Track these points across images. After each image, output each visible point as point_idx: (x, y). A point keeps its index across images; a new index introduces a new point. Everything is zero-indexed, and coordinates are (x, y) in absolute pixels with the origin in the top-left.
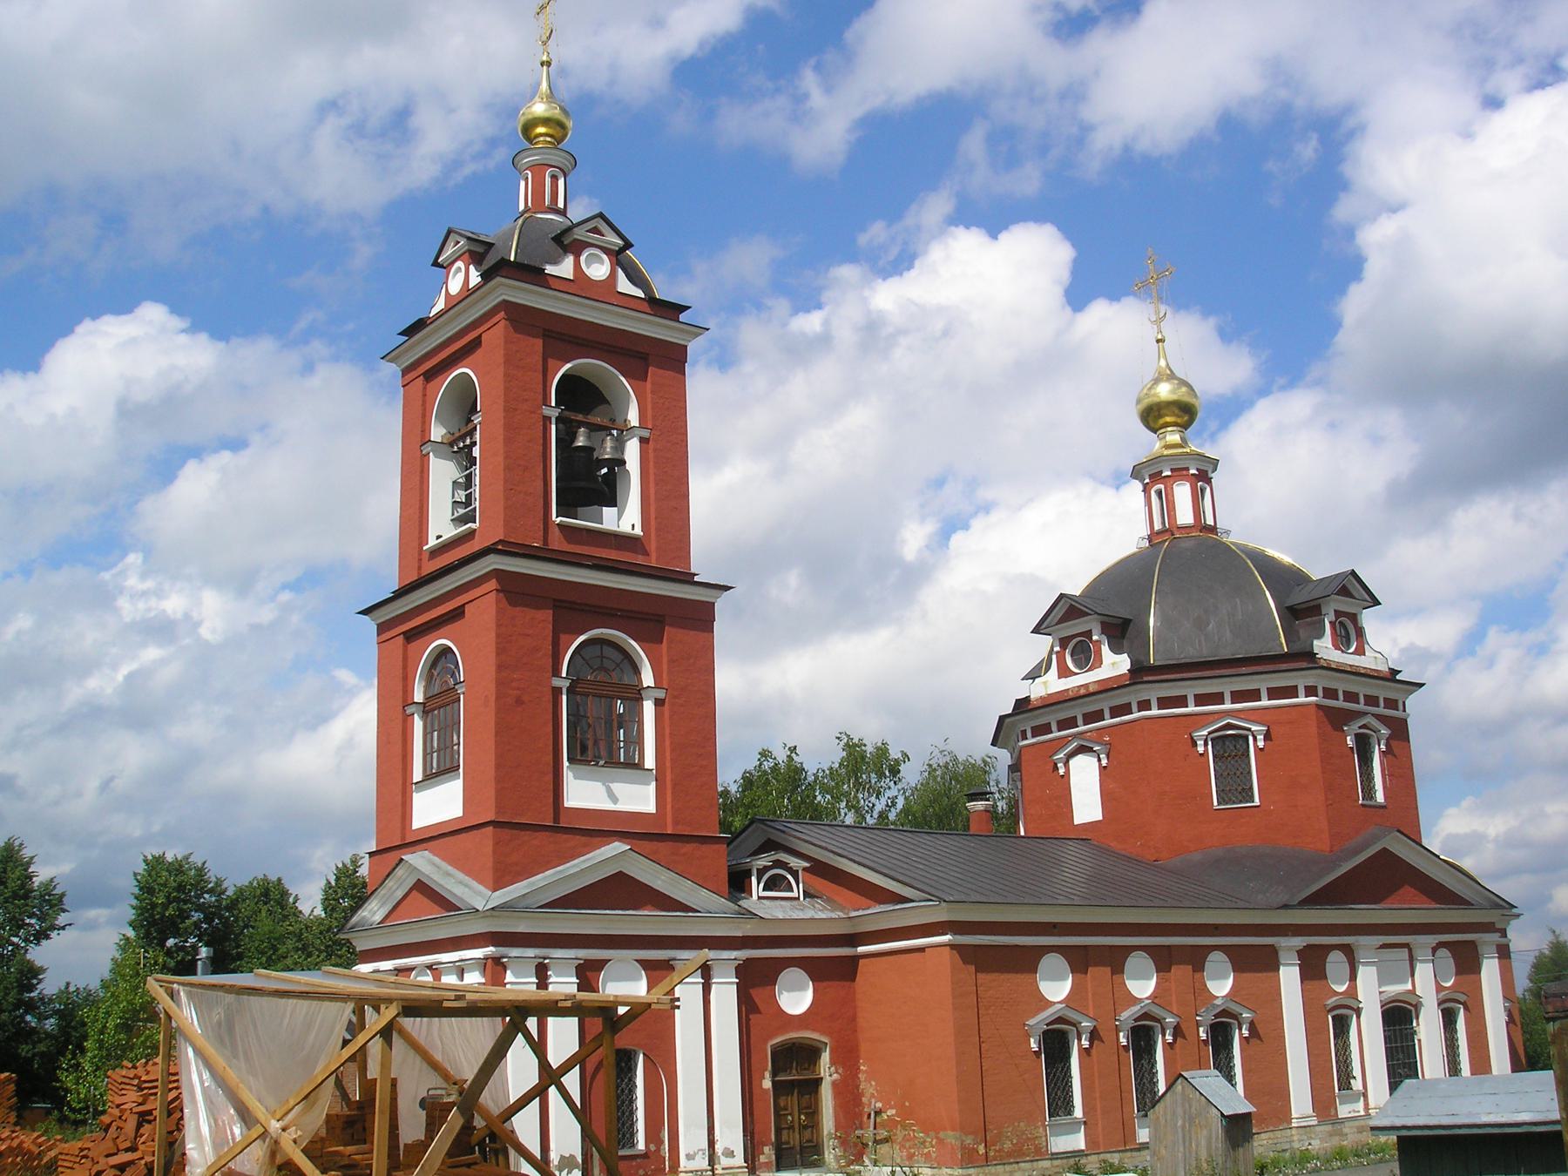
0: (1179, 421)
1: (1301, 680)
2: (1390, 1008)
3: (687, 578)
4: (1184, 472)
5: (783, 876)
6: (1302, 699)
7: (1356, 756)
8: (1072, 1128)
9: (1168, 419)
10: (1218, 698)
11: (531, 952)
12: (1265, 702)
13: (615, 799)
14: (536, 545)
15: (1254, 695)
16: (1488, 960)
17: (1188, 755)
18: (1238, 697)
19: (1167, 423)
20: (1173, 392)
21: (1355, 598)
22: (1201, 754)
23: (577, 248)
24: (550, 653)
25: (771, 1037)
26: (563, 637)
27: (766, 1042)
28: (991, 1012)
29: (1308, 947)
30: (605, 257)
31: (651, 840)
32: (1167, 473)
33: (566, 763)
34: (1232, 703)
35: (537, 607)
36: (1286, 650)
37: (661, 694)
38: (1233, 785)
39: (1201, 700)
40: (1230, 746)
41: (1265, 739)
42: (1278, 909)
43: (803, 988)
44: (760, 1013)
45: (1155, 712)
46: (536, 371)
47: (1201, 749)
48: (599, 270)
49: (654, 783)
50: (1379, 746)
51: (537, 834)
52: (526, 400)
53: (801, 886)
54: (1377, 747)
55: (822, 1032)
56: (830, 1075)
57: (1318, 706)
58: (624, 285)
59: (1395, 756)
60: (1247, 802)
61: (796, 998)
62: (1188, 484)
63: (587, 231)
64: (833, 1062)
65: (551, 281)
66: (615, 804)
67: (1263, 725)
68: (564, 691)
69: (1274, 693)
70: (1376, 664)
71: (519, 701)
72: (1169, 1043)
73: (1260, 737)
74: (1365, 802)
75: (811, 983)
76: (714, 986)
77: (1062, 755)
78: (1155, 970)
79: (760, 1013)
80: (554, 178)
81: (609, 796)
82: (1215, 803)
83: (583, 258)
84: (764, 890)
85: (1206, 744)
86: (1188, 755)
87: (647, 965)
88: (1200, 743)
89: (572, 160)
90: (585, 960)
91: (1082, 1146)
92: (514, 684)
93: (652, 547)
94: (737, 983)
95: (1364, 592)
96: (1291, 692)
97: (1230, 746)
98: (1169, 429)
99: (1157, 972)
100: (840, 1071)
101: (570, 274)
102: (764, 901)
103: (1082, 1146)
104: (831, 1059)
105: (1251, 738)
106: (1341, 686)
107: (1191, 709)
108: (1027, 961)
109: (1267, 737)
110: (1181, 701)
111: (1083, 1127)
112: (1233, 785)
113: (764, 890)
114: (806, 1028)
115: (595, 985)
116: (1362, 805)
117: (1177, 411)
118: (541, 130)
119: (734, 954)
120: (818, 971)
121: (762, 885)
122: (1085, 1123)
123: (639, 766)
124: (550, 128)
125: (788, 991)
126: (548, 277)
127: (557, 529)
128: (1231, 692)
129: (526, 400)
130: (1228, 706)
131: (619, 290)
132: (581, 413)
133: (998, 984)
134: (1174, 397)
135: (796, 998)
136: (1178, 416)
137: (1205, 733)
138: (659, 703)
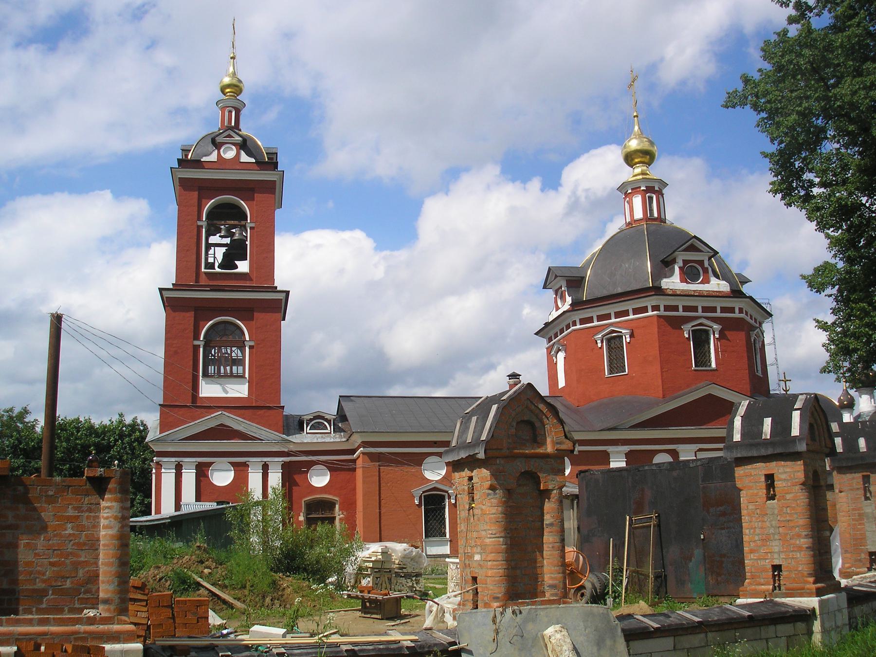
0: (643, 160)
1: (649, 302)
2: (430, 495)
3: (274, 289)
4: (638, 189)
5: (321, 422)
6: (650, 313)
7: (692, 342)
8: (443, 544)
9: (636, 160)
10: (607, 317)
11: (173, 459)
12: (631, 317)
13: (227, 392)
14: (191, 283)
15: (625, 313)
16: (613, 463)
17: (594, 349)
18: (618, 315)
19: (636, 162)
20: (638, 144)
21: (703, 252)
22: (600, 348)
23: (217, 145)
24: (193, 330)
25: (305, 497)
26: (201, 323)
27: (301, 499)
28: (388, 485)
29: (631, 451)
30: (234, 147)
31: (241, 409)
32: (630, 191)
33: (201, 378)
34: (580, 325)
35: (187, 311)
36: (651, 286)
37: (252, 343)
38: (616, 364)
39: (600, 318)
40: (614, 341)
41: (631, 337)
42: (601, 430)
43: (326, 475)
44: (299, 486)
45: (578, 327)
46: (194, 206)
47: (599, 345)
48: (230, 154)
49: (247, 384)
50: (714, 335)
51: (181, 409)
52: (189, 220)
53: (332, 427)
54: (712, 336)
55: (335, 495)
56: (339, 515)
57: (659, 316)
58: (244, 158)
59: (728, 340)
60: (623, 372)
61: (320, 479)
62: (640, 196)
63: (224, 137)
64: (340, 509)
65: (206, 166)
66: (227, 394)
67: (628, 330)
68: (202, 346)
69: (636, 311)
70: (719, 288)
71: (176, 353)
72: (417, 505)
73: (628, 336)
74: (697, 368)
75: (329, 472)
76: (269, 473)
77: (553, 353)
78: (570, 464)
79: (299, 486)
80: (230, 112)
81: (223, 391)
82: (606, 374)
83: (221, 150)
84: (310, 430)
85: (602, 342)
86: (594, 349)
87: (233, 464)
88: (599, 342)
89: (242, 104)
90: (198, 462)
91: (449, 553)
92: (174, 346)
93: (254, 277)
94: (626, 461)
95: (706, 248)
96: (644, 310)
97: (614, 341)
98: (638, 165)
99: (571, 465)
100: (345, 513)
101: (215, 158)
102: (309, 435)
103: (449, 553)
104: (339, 508)
105: (624, 337)
106: (681, 303)
107: (596, 323)
108: (418, 460)
109: (632, 336)
110: (590, 320)
111: (449, 543)
112: (616, 364)
113: (310, 430)
114: (326, 493)
115: (206, 473)
116: (695, 370)
117: (641, 155)
118: (228, 90)
119: (281, 459)
120: (332, 468)
121: (309, 428)
122: (450, 541)
123: (243, 377)
124: (232, 88)
125: (316, 476)
126: (203, 163)
127: (204, 275)
128: (633, 309)
129: (189, 220)
130: (613, 320)
131: (241, 161)
132: (223, 220)
133: (391, 472)
134: (639, 148)
135: (320, 479)
136: (642, 157)
137: (600, 336)
138: (251, 347)
